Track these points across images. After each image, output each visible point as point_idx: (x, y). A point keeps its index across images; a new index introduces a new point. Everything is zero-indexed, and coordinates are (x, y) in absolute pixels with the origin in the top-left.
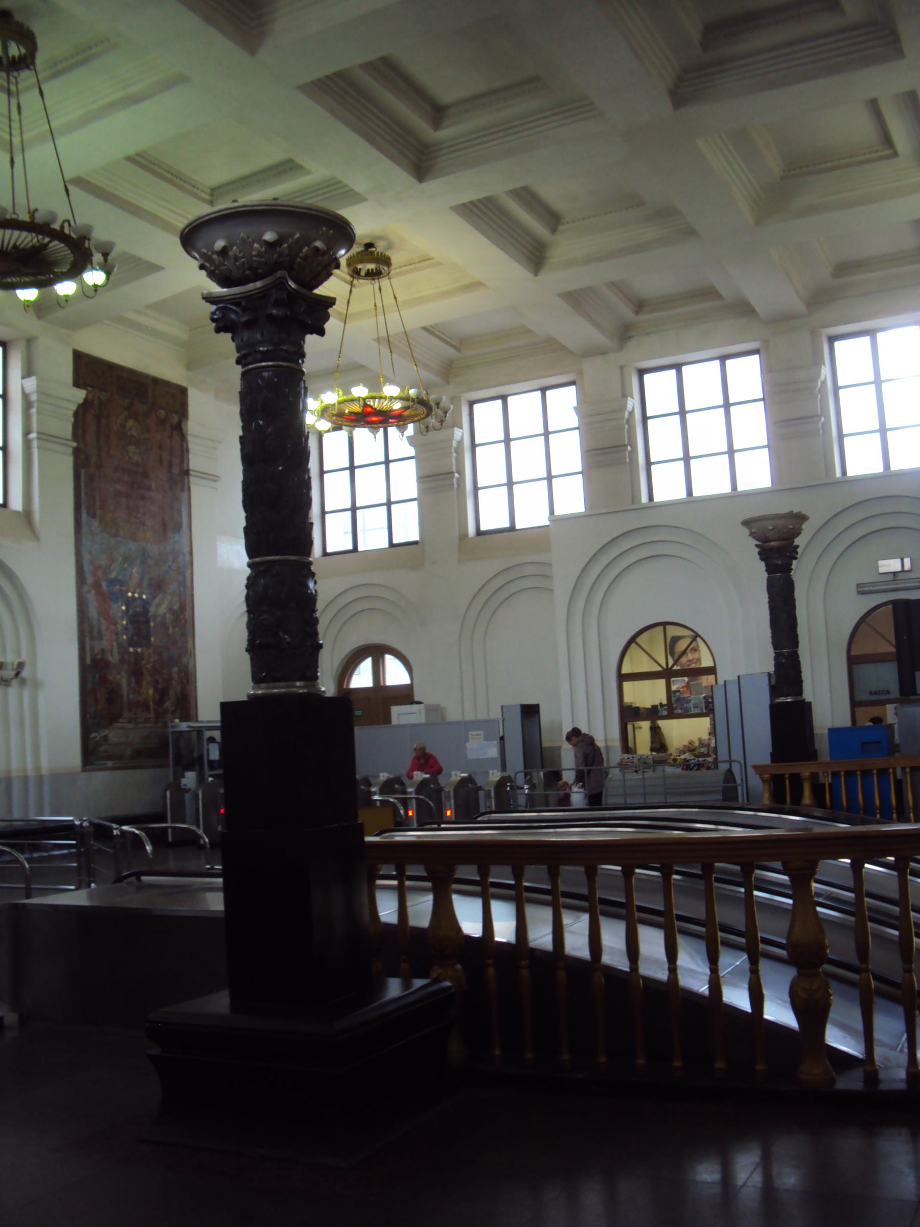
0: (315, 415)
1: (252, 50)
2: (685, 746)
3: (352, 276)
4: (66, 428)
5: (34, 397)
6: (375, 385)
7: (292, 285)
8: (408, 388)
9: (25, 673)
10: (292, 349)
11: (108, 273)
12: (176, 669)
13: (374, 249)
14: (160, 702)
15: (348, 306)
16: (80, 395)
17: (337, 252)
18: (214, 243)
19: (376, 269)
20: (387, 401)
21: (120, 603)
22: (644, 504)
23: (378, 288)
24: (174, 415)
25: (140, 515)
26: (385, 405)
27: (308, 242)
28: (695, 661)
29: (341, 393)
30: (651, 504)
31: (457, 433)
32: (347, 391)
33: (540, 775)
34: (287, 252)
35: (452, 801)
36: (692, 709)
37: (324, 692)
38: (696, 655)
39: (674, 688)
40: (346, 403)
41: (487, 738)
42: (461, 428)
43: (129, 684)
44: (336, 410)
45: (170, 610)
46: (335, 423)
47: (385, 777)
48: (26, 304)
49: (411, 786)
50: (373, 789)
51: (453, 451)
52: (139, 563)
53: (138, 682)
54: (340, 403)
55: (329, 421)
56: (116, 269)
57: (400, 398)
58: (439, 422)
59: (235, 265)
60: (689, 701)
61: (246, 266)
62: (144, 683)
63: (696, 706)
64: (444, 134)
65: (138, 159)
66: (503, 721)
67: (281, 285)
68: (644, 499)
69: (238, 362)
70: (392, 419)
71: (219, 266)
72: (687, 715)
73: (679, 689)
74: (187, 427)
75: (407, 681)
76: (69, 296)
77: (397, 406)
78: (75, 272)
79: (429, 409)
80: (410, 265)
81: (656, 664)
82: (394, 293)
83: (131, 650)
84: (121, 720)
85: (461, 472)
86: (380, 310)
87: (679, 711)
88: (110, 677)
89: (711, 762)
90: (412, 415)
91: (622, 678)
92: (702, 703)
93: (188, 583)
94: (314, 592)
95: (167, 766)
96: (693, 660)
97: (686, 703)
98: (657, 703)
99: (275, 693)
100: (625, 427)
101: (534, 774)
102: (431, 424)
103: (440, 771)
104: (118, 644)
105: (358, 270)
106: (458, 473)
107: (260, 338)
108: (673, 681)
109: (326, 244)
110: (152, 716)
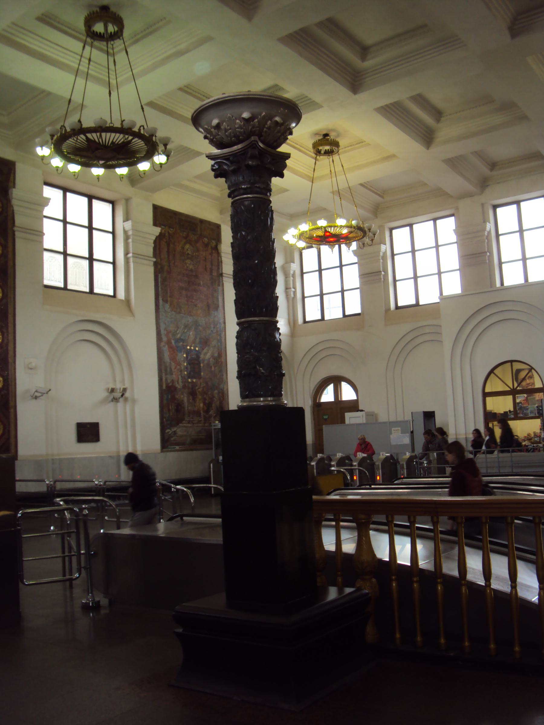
0: (296, 238)
1: (250, 18)
2: (525, 437)
3: (316, 154)
4: (150, 251)
5: (130, 233)
6: (331, 219)
7: (261, 145)
8: (351, 220)
9: (127, 394)
10: (262, 186)
11: (168, 156)
12: (216, 391)
13: (329, 137)
14: (207, 411)
15: (314, 172)
16: (157, 231)
17: (290, 125)
18: (212, 121)
19: (331, 149)
20: (338, 229)
21: (183, 353)
22: (498, 287)
23: (332, 160)
24: (213, 241)
25: (193, 301)
26: (337, 231)
27: (271, 118)
28: (531, 384)
29: (311, 224)
30: (503, 287)
31: (383, 247)
32: (314, 223)
33: (434, 455)
34: (257, 124)
35: (381, 471)
36: (529, 414)
37: (286, 404)
38: (531, 381)
39: (518, 401)
40: (314, 230)
41: (403, 432)
42: (385, 244)
43: (188, 400)
44: (308, 235)
45: (212, 356)
46: (308, 243)
47: (340, 457)
48: (121, 176)
49: (355, 462)
50: (333, 463)
51: (380, 258)
52: (193, 329)
53: (194, 399)
54: (310, 230)
55: (304, 242)
56: (172, 154)
57: (347, 227)
58: (371, 240)
59: (226, 134)
60: (527, 409)
61: (232, 135)
62: (198, 400)
63: (531, 412)
64: (368, 64)
65: (186, 89)
66: (412, 421)
67: (254, 146)
68: (498, 284)
69: (229, 196)
70: (342, 239)
71: (216, 136)
72: (526, 417)
73: (521, 402)
74: (221, 248)
75: (355, 398)
76: (145, 171)
77: (345, 231)
78: (149, 156)
79: (365, 233)
80: (351, 146)
81: (507, 387)
82: (341, 163)
83: (190, 380)
84: (184, 422)
85: (386, 271)
86: (333, 174)
87: (521, 415)
88: (177, 397)
89: (541, 447)
90: (355, 237)
91: (485, 395)
92: (535, 410)
93: (223, 340)
94: (279, 340)
95: (211, 449)
96: (529, 384)
97: (525, 410)
98: (507, 410)
99: (255, 405)
100: (485, 241)
101: (431, 454)
102: (366, 242)
103: (374, 453)
104: (182, 377)
105: (320, 150)
106: (384, 272)
107: (242, 180)
108: (517, 396)
109: (282, 119)
110: (202, 419)
